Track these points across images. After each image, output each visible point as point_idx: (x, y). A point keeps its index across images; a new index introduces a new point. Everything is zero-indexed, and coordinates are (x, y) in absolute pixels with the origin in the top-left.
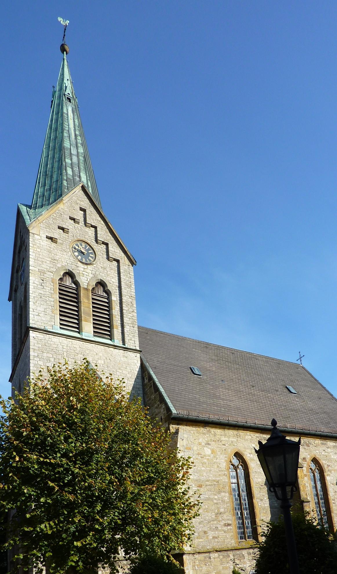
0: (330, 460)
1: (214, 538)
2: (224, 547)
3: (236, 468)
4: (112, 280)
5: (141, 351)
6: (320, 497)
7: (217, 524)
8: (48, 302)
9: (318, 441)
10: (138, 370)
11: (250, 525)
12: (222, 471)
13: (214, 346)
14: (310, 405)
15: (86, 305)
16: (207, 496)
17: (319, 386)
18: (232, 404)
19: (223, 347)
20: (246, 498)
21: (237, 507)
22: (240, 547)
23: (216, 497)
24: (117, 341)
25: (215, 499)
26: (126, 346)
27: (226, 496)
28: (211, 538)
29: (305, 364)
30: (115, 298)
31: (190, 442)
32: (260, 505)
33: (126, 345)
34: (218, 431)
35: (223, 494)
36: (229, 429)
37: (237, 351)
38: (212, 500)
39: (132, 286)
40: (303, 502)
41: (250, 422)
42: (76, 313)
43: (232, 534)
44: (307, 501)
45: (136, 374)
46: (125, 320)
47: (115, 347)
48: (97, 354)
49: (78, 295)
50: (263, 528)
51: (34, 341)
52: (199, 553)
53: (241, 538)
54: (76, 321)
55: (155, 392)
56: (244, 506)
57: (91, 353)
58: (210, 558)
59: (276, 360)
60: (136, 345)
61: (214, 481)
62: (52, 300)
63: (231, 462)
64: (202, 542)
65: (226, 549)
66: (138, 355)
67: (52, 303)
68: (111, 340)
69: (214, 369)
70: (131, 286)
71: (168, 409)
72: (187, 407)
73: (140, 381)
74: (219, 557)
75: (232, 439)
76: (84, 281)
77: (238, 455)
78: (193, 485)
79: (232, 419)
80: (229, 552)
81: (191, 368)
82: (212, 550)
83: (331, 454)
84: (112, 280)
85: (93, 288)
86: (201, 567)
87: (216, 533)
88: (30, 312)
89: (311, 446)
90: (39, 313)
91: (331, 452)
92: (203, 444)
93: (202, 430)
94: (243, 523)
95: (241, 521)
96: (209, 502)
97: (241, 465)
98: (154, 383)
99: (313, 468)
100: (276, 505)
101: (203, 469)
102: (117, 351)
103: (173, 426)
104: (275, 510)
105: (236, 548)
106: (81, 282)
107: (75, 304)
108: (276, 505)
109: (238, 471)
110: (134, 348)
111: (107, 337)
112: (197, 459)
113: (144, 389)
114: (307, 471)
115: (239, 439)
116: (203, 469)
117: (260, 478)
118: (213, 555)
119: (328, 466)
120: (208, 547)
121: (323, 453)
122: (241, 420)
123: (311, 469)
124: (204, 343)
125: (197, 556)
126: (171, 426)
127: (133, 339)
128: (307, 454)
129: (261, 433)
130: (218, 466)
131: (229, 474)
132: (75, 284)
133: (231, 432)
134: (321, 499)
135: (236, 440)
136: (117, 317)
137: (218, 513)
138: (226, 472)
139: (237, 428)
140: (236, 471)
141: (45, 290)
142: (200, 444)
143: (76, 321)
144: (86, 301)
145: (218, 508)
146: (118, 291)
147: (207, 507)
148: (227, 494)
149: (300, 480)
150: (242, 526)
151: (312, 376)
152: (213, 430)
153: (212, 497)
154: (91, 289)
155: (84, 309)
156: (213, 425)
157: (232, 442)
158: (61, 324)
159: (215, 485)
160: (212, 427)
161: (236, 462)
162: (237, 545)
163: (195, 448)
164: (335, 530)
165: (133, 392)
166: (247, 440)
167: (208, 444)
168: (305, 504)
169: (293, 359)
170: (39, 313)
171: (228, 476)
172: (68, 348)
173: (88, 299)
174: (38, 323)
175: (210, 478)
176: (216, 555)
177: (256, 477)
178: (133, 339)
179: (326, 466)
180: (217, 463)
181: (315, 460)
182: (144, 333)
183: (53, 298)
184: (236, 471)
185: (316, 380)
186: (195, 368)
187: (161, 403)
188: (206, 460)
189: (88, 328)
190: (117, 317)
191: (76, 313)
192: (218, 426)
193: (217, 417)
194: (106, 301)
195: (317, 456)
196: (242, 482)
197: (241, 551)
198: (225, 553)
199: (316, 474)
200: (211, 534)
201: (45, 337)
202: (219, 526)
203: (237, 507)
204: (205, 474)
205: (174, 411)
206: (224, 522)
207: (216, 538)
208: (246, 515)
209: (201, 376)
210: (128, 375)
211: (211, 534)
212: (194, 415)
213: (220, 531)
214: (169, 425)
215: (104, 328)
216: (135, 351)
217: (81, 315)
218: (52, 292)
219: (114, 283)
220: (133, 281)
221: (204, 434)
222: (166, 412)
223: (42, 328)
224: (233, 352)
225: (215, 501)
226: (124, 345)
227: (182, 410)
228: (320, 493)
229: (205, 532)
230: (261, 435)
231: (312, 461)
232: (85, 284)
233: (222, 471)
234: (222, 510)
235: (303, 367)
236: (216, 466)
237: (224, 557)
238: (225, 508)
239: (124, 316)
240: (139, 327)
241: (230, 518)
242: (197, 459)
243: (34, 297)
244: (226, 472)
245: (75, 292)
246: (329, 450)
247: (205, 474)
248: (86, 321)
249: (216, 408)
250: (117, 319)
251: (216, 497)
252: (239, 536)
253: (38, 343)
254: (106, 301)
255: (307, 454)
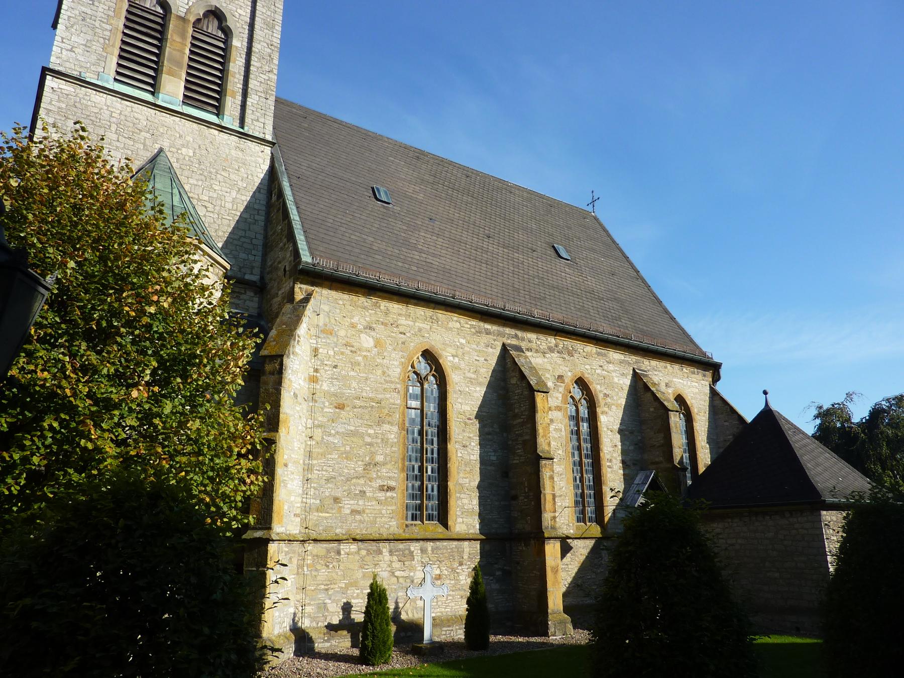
0: (611, 386)
1: (353, 512)
2: (374, 533)
3: (421, 380)
4: (239, 11)
5: (274, 144)
6: (584, 452)
7: (364, 485)
8: (97, 30)
9: (591, 349)
10: (262, 176)
11: (436, 492)
12: (392, 382)
13: (435, 157)
14: (592, 282)
15: (178, 47)
16: (353, 428)
17: (618, 253)
18: (436, 262)
19: (451, 163)
20: (435, 439)
21: (414, 455)
22: (407, 536)
23: (371, 431)
24: (230, 119)
25: (369, 435)
26: (246, 130)
27: (392, 432)
28: (348, 511)
29: (603, 213)
30: (238, 43)
31: (333, 321)
32: (460, 455)
33: (246, 128)
34: (395, 307)
35: (386, 427)
36: (416, 305)
37: (477, 173)
38: (362, 436)
39: (277, 27)
40: (540, 458)
41: (462, 297)
42: (155, 59)
43: (394, 508)
44: (548, 456)
45: (257, 184)
46: (252, 84)
47: (222, 128)
48: (180, 136)
49: (164, 26)
50: (610, 504)
51: (52, 96)
52: (315, 540)
53: (578, 520)
54: (152, 73)
55: (284, 220)
56: (429, 455)
57: (169, 132)
58: (339, 553)
59: (548, 198)
60: (267, 131)
61: (372, 399)
62: (109, 27)
63: (413, 367)
64: (326, 518)
65: (377, 536)
66: (268, 150)
67: (107, 33)
68: (217, 115)
69: (421, 196)
70: (273, 27)
71: (296, 254)
72: (340, 254)
73: (263, 197)
74: (358, 553)
75: (421, 325)
76: (181, 4)
77: (429, 356)
78: (327, 404)
79: (424, 289)
80: (381, 544)
81: (373, 188)
82: (344, 537)
83: (614, 374)
84: (239, 11)
85: (199, 20)
86: (316, 570)
87: (361, 502)
88: (55, 43)
89: (576, 355)
90: (73, 47)
91: (615, 371)
92: (360, 327)
93: (362, 300)
94: (421, 488)
95: (417, 484)
96: (355, 440)
97: (433, 375)
98: (284, 204)
99: (577, 397)
100: (494, 458)
101: (352, 373)
102: (226, 136)
103: (304, 286)
104: (489, 468)
105: (396, 537)
106: (175, 4)
107: (155, 42)
108: (494, 458)
109: (426, 386)
110: (261, 136)
111: (210, 109)
112: (342, 353)
113: (268, 214)
114: (565, 401)
115: (435, 326)
116: (352, 373)
117: (467, 404)
118: (345, 548)
119: (606, 395)
120: (338, 531)
121: (599, 371)
122: (443, 291)
123: (572, 397)
124: (416, 150)
125: (310, 547)
126: (298, 287)
127: (262, 120)
128: (567, 369)
129: (481, 320)
130: (384, 373)
131: (408, 390)
132: (162, 7)
133: (420, 311)
134: (587, 456)
135: (429, 327)
136: (237, 76)
137: (370, 463)
138: (398, 386)
139: (432, 305)
140: (422, 385)
141: (95, 8)
142: (353, 326)
143: (152, 73)
144: (178, 39)
145: (373, 454)
146: (247, 32)
147: (348, 448)
148: (395, 429)
149: (540, 417)
150: (420, 493)
151: (609, 235)
152: (384, 304)
153: (362, 430)
154: (192, 19)
155: (170, 53)
156: (385, 295)
157: (420, 330)
158: (118, 73)
159: (372, 407)
160: (383, 298)
161: (423, 367)
162: (401, 531)
163: (342, 333)
164: (606, 519)
165: (245, 216)
166: (451, 329)
167: (370, 328)
168: (543, 462)
169: (582, 203)
170: (73, 47)
171: (402, 393)
172: (123, 118)
173: (183, 35)
174: (67, 65)
175: (364, 394)
176: (354, 547)
177: (459, 400)
178: (262, 120)
179: (601, 396)
180: (382, 366)
181: (581, 383)
182: (286, 112)
183: (111, 24)
184: (422, 385)
185: (614, 242)
186: (382, 189)
187: (288, 241)
188: (360, 358)
189: (173, 88)
190: (237, 76)
191: (155, 59)
192: (395, 297)
193: (397, 280)
194: (222, 45)
195: (586, 375)
196: (431, 408)
197: (408, 543)
198: (373, 546)
199: (581, 409)
200: (348, 505)
201: (78, 91)
202: (368, 489)
203: (414, 455)
204: (354, 384)
205: (306, 257)
206: (380, 482)
207: (358, 512)
208: (429, 472)
209: (390, 206)
210: (240, 183)
211: (348, 505)
212: (347, 270)
213: (370, 499)
214: (294, 283)
215: (207, 90)
216: (263, 141)
217: (163, 63)
218: (111, 14)
219: (242, 18)
220: (279, 18)
221: (365, 308)
222: (292, 258)
223: (75, 74)
224: (468, 173)
225: (368, 440)
226: (242, 128)
227: (321, 257)
228: (586, 446)
229: (336, 500)
230: (482, 324)
231: (576, 382)
232: (181, 9)
233: (392, 382)
234: (379, 458)
235: (596, 218)
236: (379, 372)
237: (369, 552)
238: (386, 455)
239: (251, 76)
240: (278, 101)
241: (394, 474)
242: (342, 353)
243: (69, 17)
244: (398, 386)
245: (159, 20)
246: (611, 367)
247: (354, 384)
248: (170, 73)
249: (400, 264)
250: (236, 80)
251: (371, 431)
252: (410, 513)
253: (59, 101)
254: (222, 45)
255: (567, 369)
